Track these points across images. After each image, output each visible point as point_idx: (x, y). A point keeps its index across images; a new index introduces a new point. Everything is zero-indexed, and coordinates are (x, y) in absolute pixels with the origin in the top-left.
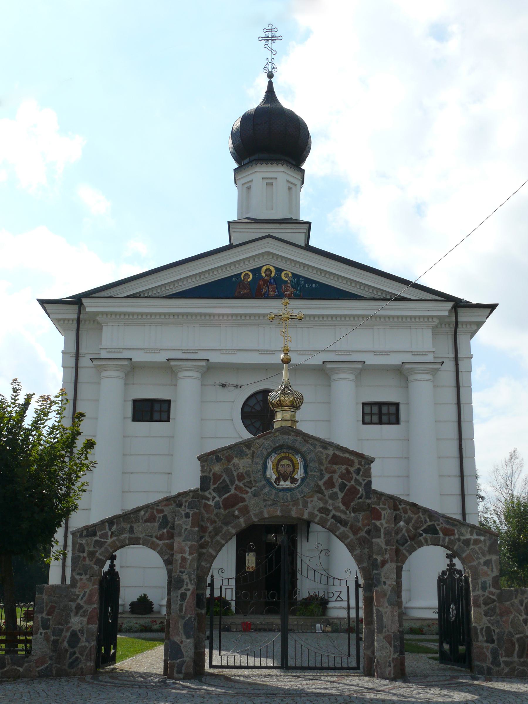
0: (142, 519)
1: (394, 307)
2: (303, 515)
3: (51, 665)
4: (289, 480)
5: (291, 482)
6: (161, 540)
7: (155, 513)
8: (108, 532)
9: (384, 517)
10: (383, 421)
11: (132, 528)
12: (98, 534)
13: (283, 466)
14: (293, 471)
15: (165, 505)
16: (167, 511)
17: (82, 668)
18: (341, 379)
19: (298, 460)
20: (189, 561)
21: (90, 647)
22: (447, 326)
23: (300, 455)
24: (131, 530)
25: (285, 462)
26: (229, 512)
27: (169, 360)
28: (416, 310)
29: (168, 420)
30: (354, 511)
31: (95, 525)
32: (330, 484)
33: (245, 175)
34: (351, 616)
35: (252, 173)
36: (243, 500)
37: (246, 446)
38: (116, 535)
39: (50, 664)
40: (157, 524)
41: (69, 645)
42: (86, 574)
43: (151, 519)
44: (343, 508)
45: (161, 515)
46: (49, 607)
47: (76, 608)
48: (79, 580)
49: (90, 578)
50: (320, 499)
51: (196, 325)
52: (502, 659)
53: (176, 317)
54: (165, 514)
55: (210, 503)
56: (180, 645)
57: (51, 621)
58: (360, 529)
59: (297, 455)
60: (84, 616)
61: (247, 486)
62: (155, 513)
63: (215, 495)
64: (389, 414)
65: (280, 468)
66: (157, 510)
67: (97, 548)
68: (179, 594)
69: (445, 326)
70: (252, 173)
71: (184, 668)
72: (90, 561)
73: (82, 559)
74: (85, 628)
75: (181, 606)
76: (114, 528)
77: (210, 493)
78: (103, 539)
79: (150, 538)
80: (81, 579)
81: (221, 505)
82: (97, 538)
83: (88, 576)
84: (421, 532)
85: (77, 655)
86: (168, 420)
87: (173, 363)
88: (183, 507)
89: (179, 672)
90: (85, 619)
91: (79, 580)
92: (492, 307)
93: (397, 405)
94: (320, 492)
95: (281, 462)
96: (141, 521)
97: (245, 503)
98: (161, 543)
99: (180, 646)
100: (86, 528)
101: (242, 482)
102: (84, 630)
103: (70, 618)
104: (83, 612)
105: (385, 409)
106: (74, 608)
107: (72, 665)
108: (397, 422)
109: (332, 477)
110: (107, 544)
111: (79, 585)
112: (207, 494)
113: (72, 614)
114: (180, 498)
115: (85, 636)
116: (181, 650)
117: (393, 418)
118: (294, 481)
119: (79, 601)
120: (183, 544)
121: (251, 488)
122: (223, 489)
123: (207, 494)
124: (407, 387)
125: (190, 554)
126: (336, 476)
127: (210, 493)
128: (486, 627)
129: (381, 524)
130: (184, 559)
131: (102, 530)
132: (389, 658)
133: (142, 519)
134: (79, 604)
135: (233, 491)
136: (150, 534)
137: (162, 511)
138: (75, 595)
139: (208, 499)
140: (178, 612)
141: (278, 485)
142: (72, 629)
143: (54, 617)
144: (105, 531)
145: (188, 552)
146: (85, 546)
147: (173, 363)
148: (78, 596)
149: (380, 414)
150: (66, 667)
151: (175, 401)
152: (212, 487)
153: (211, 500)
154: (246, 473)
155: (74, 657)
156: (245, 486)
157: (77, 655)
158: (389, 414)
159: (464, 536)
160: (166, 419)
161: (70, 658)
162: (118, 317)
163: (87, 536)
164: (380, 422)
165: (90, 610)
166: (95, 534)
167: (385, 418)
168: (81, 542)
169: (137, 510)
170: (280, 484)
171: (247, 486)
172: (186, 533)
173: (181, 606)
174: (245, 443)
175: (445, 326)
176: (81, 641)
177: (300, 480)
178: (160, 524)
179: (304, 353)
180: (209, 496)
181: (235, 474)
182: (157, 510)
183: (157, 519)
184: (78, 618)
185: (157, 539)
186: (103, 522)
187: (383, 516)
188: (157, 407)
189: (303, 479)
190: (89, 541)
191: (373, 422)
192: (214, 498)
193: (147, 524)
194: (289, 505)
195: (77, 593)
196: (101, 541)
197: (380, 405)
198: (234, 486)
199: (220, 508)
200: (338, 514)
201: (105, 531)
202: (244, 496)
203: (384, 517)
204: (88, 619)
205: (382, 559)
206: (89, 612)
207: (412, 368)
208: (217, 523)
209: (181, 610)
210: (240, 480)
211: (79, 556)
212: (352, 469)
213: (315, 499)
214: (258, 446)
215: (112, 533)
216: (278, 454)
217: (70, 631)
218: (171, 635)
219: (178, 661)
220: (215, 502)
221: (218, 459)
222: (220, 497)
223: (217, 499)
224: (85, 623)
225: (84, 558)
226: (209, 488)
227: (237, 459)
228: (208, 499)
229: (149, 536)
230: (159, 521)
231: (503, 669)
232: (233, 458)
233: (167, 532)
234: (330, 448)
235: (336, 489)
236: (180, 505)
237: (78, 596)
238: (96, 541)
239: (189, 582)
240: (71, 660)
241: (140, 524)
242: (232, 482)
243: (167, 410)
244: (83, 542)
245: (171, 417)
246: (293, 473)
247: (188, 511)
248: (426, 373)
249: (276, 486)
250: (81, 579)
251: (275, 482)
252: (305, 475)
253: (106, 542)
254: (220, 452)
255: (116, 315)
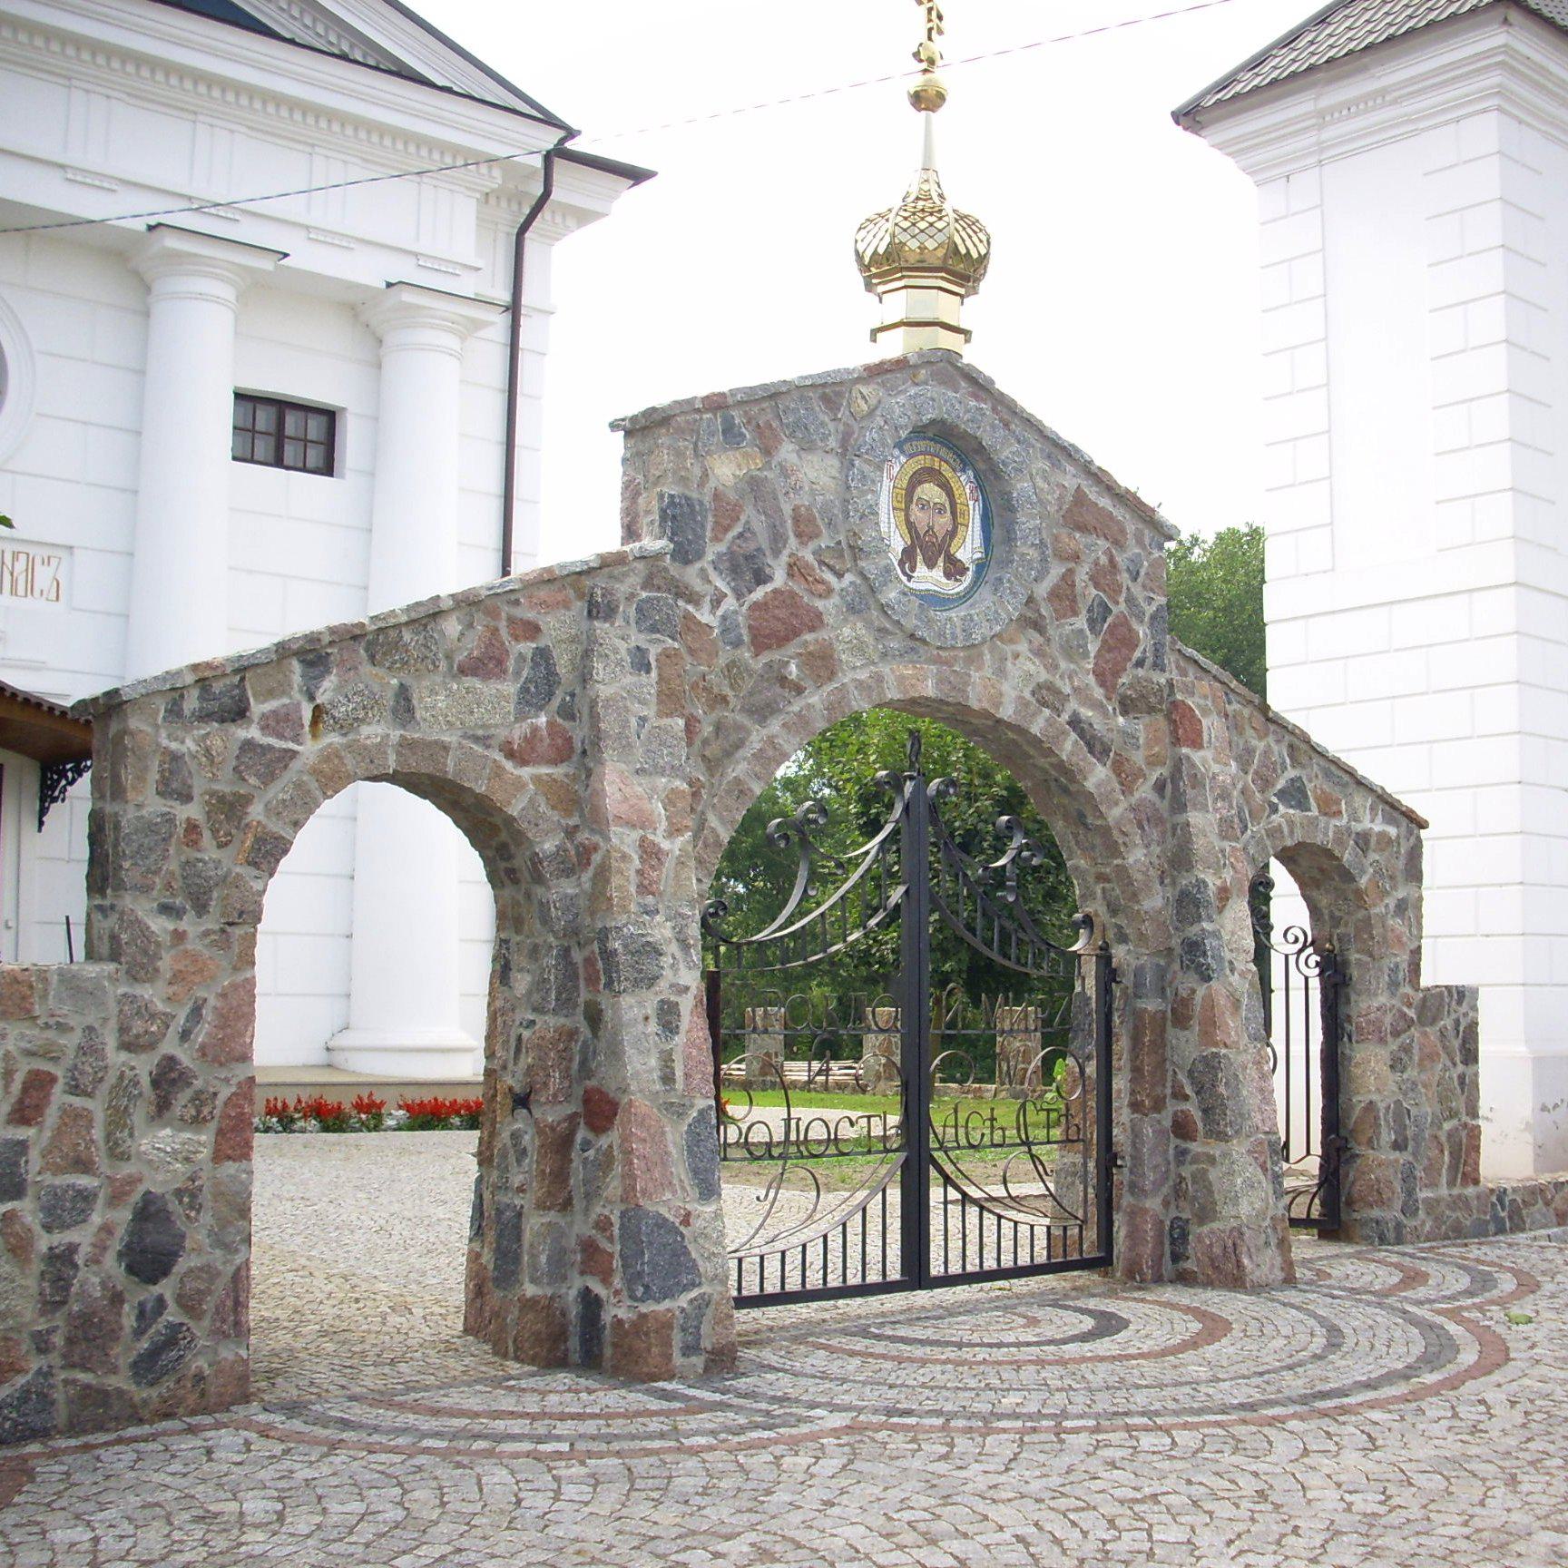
0: (448, 657)
1: (399, 100)
2: (998, 705)
3: (46, 1374)
4: (941, 563)
5: (948, 575)
6: (524, 762)
7: (504, 633)
8: (299, 704)
9: (1210, 742)
11: (403, 693)
12: (258, 708)
13: (924, 506)
14: (952, 534)
15: (543, 603)
16: (558, 626)
17: (199, 1378)
18: (201, 297)
19: (968, 491)
20: (669, 864)
21: (230, 1269)
22: (504, 204)
23: (971, 473)
24: (404, 707)
25: (930, 491)
26: (769, 665)
30: (1126, 707)
31: (244, 668)
32: (1064, 597)
36: (816, 621)
37: (825, 399)
38: (345, 727)
39: (39, 1372)
40: (510, 688)
41: (131, 1270)
42: (201, 908)
43: (486, 664)
44: (1098, 693)
45: (527, 647)
46: (19, 1078)
47: (155, 1083)
48: (165, 939)
49: (223, 931)
50: (1039, 653)
52: (1424, 1194)
54: (542, 645)
55: (704, 616)
56: (682, 1228)
57: (34, 1154)
58: (1140, 774)
59: (963, 470)
60: (197, 1121)
61: (828, 566)
62: (504, 633)
63: (721, 584)
65: (917, 514)
66: (511, 621)
67: (253, 781)
68: (650, 1009)
69: (498, 203)
71: (705, 1329)
72: (221, 846)
73: (180, 831)
74: (204, 1180)
75: (667, 1059)
76: (327, 689)
77: (703, 574)
78: (281, 736)
79: (478, 749)
80: (179, 936)
81: (746, 638)
82: (253, 733)
83: (211, 922)
84: (1275, 800)
85: (172, 1315)
88: (619, 622)
89: (689, 1350)
90: (206, 1137)
91: (165, 939)
92: (636, 175)
93: (330, 416)
94: (1038, 625)
95: (919, 489)
96: (443, 665)
97: (823, 634)
98: (526, 772)
99: (683, 1236)
100: (204, 676)
101: (812, 546)
102: (200, 1189)
103: (131, 1135)
104: (192, 1100)
105: (292, 423)
106: (145, 1081)
107: (147, 1367)
108: (328, 469)
109: (1070, 571)
110: (295, 765)
111: (166, 963)
112: (690, 575)
113: (139, 1116)
114: (600, 582)
115: (206, 1218)
116: (687, 1253)
117: (314, 456)
118: (954, 569)
119: (169, 1046)
120: (639, 787)
121: (840, 575)
122: (747, 569)
123: (690, 575)
125: (674, 831)
126: (1082, 574)
127: (703, 574)
128: (1395, 1103)
129: (1204, 761)
130: (651, 853)
131: (271, 694)
132: (1264, 1219)
133: (448, 657)
134: (171, 1061)
135: (779, 579)
136: (480, 732)
137: (532, 630)
138: (153, 1016)
139: (694, 599)
140: (658, 1087)
141: (910, 578)
142: (141, 1189)
143: (48, 1134)
144: (286, 701)
145: (664, 824)
146: (193, 766)
148: (167, 1020)
149: (280, 437)
150: (120, 1381)
152: (712, 551)
153: (707, 606)
154: (822, 511)
155: (159, 1325)
156: (821, 563)
157: (172, 1315)
159: (1360, 822)
161: (139, 1333)
163: (205, 717)
164: (278, 462)
165: (225, 1093)
166: (239, 713)
167: (290, 451)
168: (174, 746)
169: (427, 616)
170: (915, 574)
171: (828, 566)
172: (644, 732)
173: (667, 1059)
174: (824, 385)
175: (498, 203)
176: (188, 1244)
177: (972, 567)
178: (524, 690)
179: (88, 181)
180: (698, 585)
181: (787, 509)
182: (511, 621)
183: (511, 665)
184: (168, 1131)
185: (510, 755)
186: (283, 651)
187: (1206, 737)
189: (981, 567)
190: (216, 743)
192: (717, 601)
193: (470, 681)
194: (955, 658)
195: (160, 1006)
196: (270, 748)
197: (282, 406)
198: (784, 558)
199: (737, 644)
200: (1086, 713)
201: (286, 701)
202: (820, 604)
203: (1210, 742)
204: (220, 1132)
205: (1219, 882)
206: (219, 1102)
208: (731, 706)
209: (668, 1079)
210: (804, 536)
211: (169, 819)
212: (1121, 560)
213: (1023, 647)
214: (865, 407)
215: (318, 712)
216: (911, 456)
217: (136, 1197)
218: (644, 1192)
219: (683, 1300)
220: (724, 618)
221: (731, 435)
222: (739, 596)
223: (730, 603)
224: (205, 1153)
225: (192, 828)
226: (700, 555)
227: (792, 447)
228: (694, 599)
229: (476, 739)
230: (518, 673)
231: (1423, 1223)
232: (780, 442)
233: (550, 724)
234: (1069, 468)
235: (1081, 622)
236: (599, 609)
237: (167, 1020)
238: (248, 745)
239: (678, 954)
240: (145, 1344)
241: (439, 679)
242: (777, 541)
244: (184, 749)
246: (952, 539)
247: (638, 639)
248: (451, 331)
249: (904, 579)
250: (179, 936)
251: (901, 563)
252: (987, 555)
253: (294, 754)
254: (741, 403)
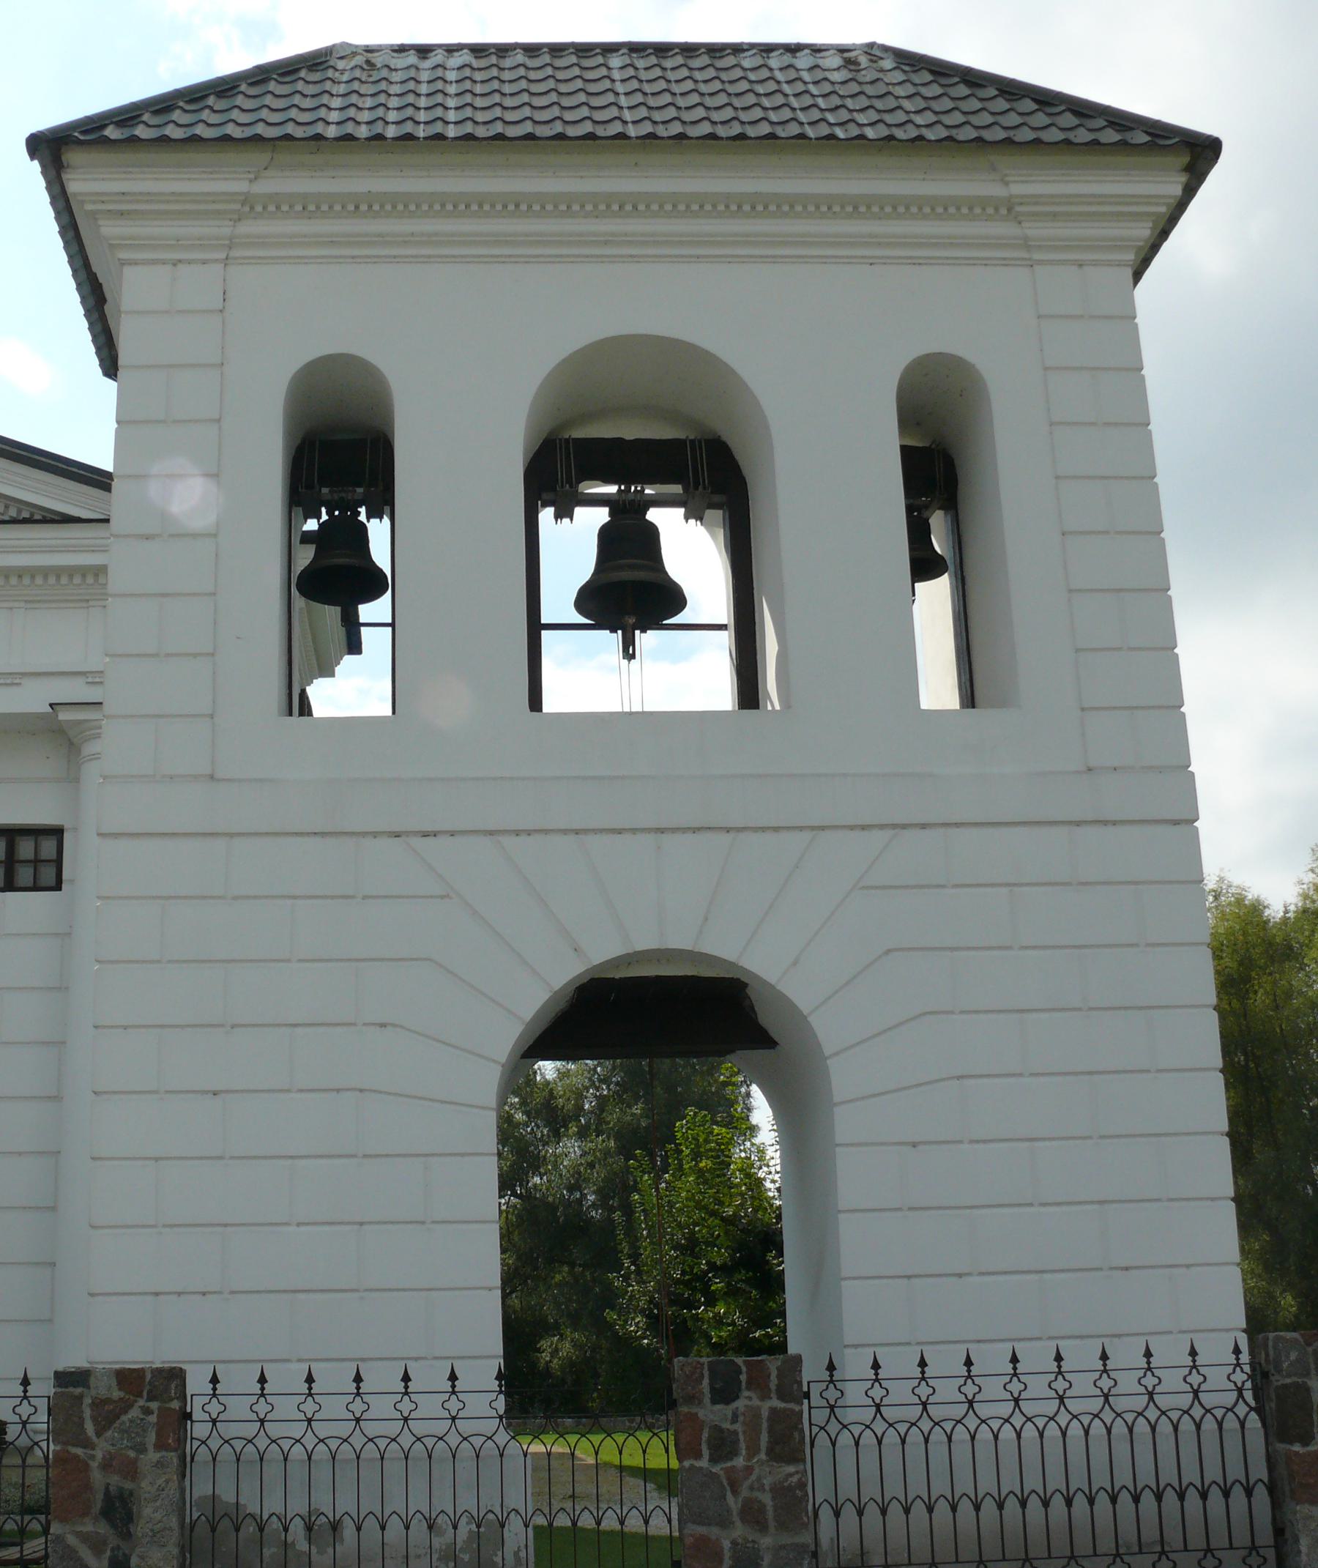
10: (20, 883)
27: (57, 708)
28: (52, 550)
29: (58, 886)
33: (1164, 179)
34: (288, 1539)
35: (173, 179)
51: (16, 605)
53: (26, 581)
64: (36, 862)
70: (173, 179)
86: (58, 886)
87: (64, 716)
124: (77, 780)
147: (64, 716)
151: (75, 829)
158: (36, 862)
160: (53, 883)
162: (77, 580)
167: (25, 874)
188: (25, 849)
191: (43, 883)
207: (79, 722)
243: (54, 857)
245: (65, 875)
255: (71, 577)
